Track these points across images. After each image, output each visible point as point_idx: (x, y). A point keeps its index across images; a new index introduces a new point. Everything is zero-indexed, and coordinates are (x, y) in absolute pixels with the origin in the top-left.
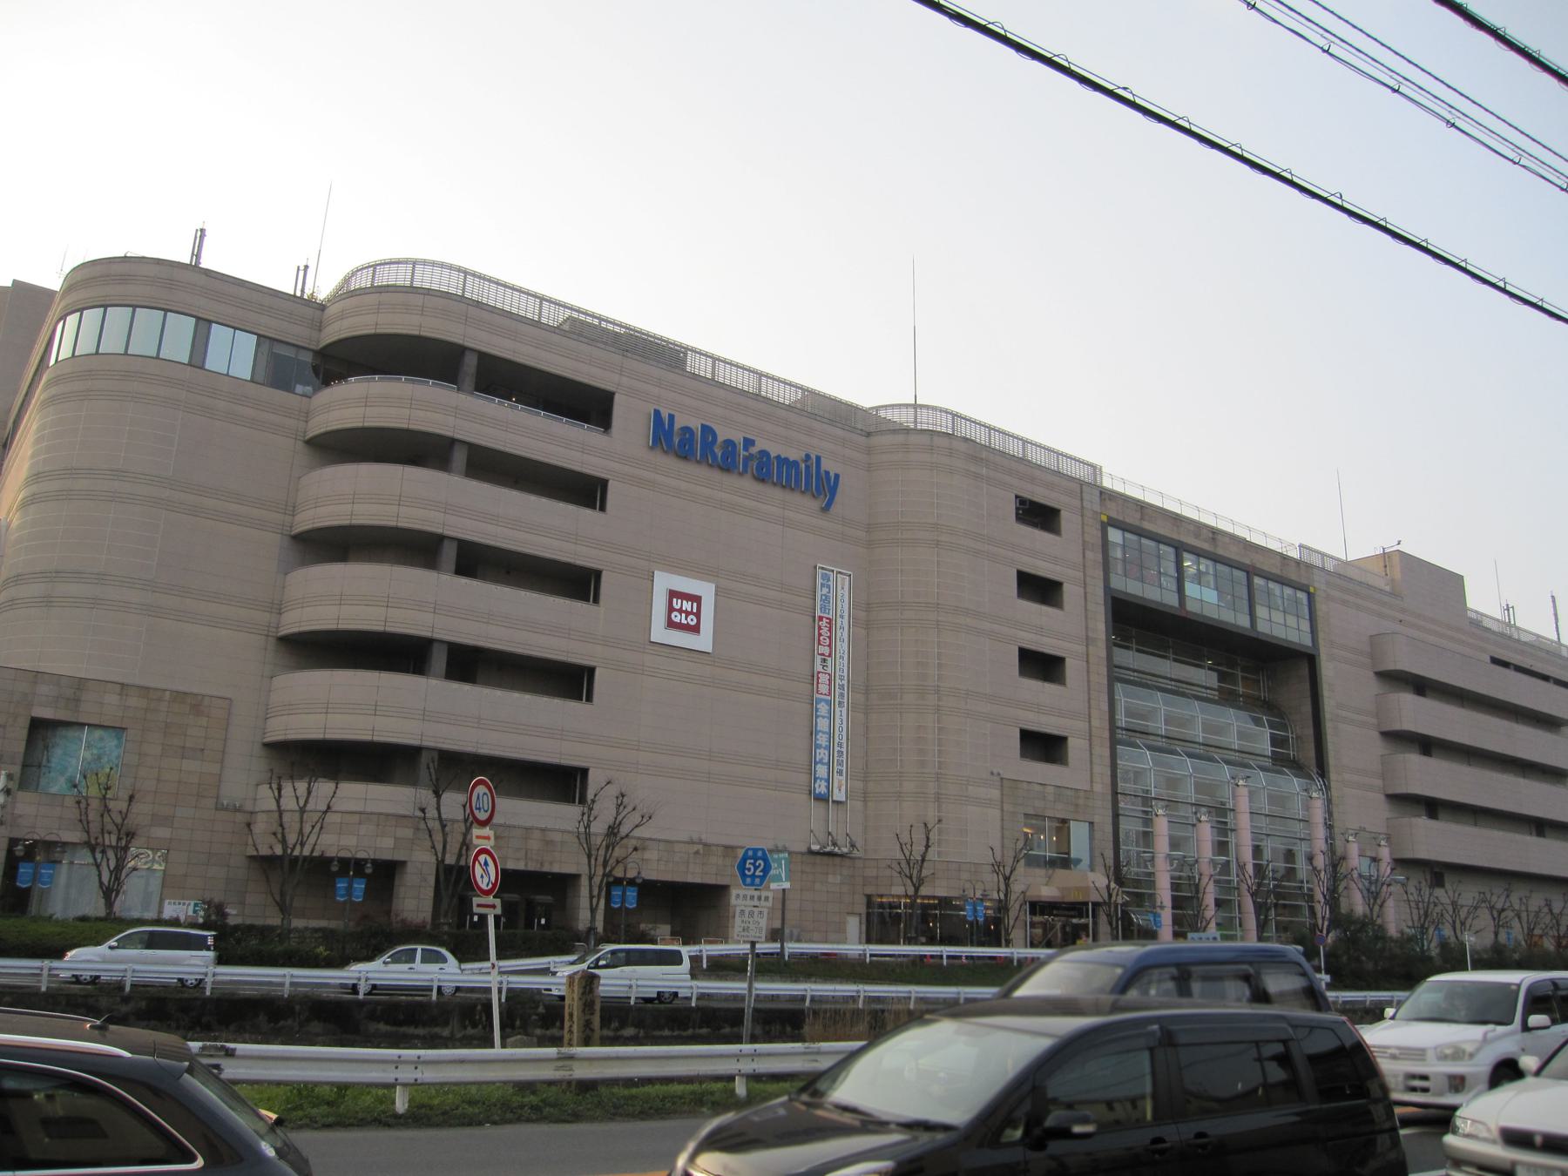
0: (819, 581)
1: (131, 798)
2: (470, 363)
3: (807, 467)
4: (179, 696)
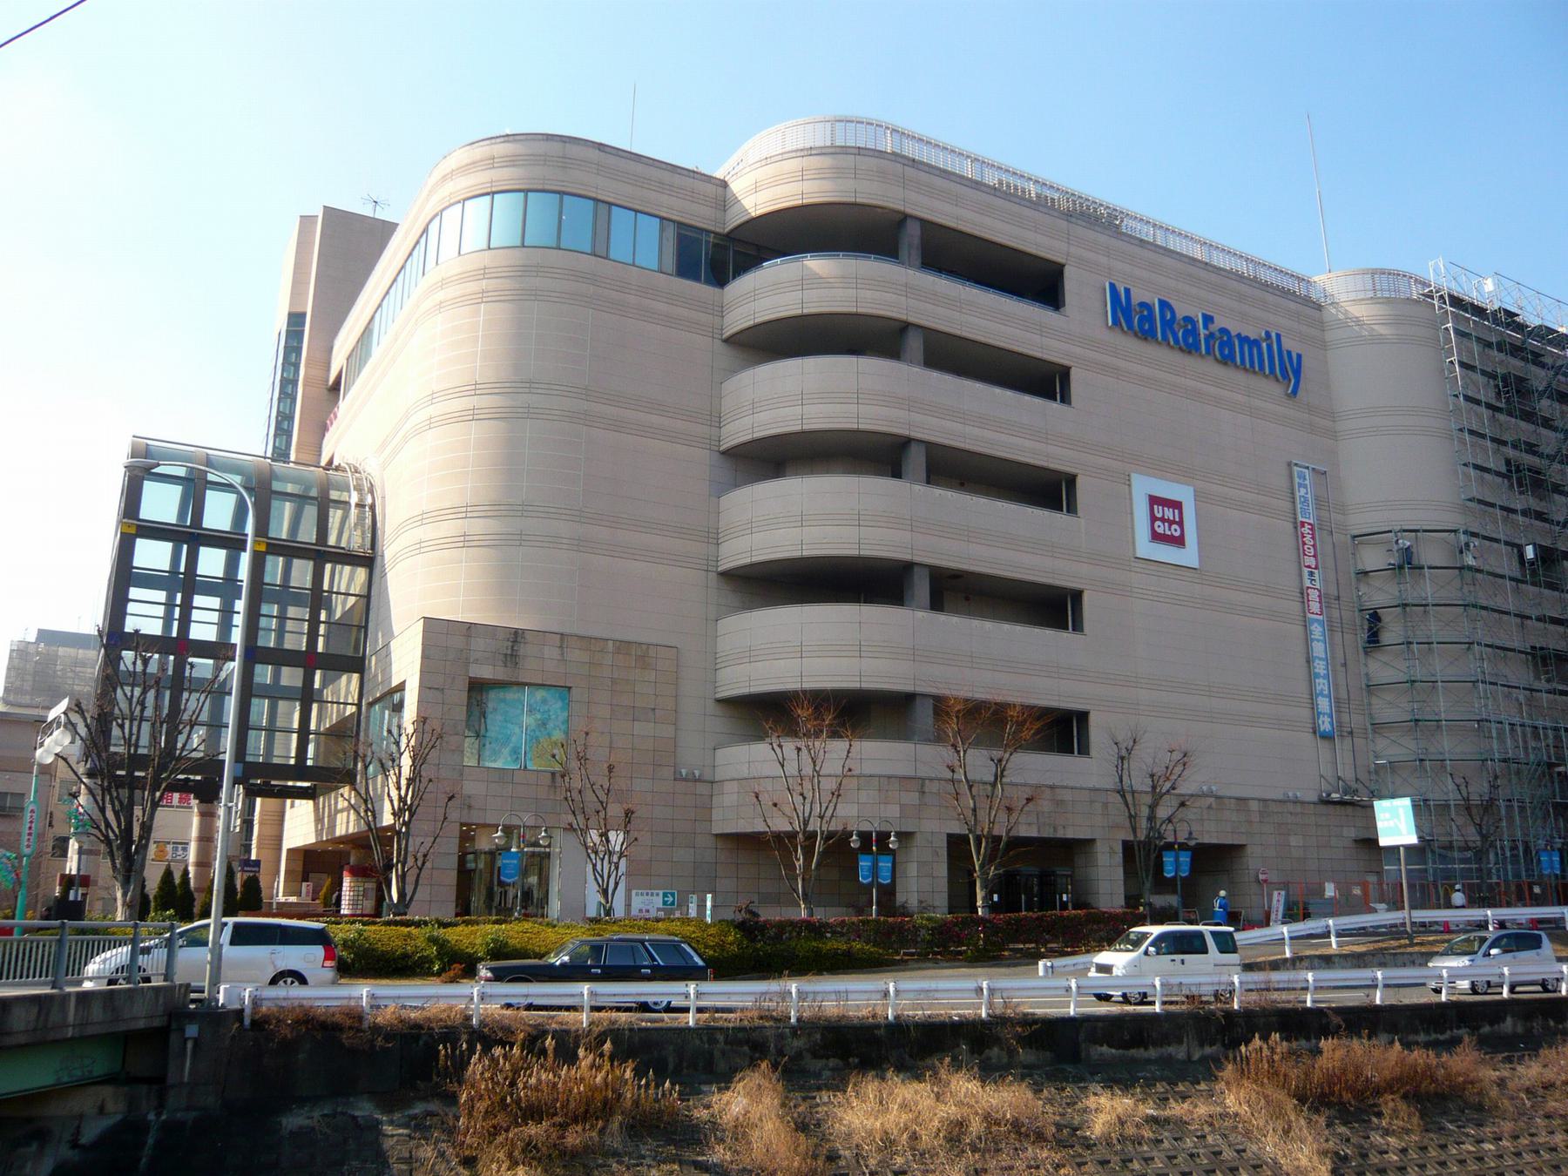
0: (1297, 480)
1: (611, 769)
2: (913, 232)
3: (1270, 347)
4: (623, 646)
